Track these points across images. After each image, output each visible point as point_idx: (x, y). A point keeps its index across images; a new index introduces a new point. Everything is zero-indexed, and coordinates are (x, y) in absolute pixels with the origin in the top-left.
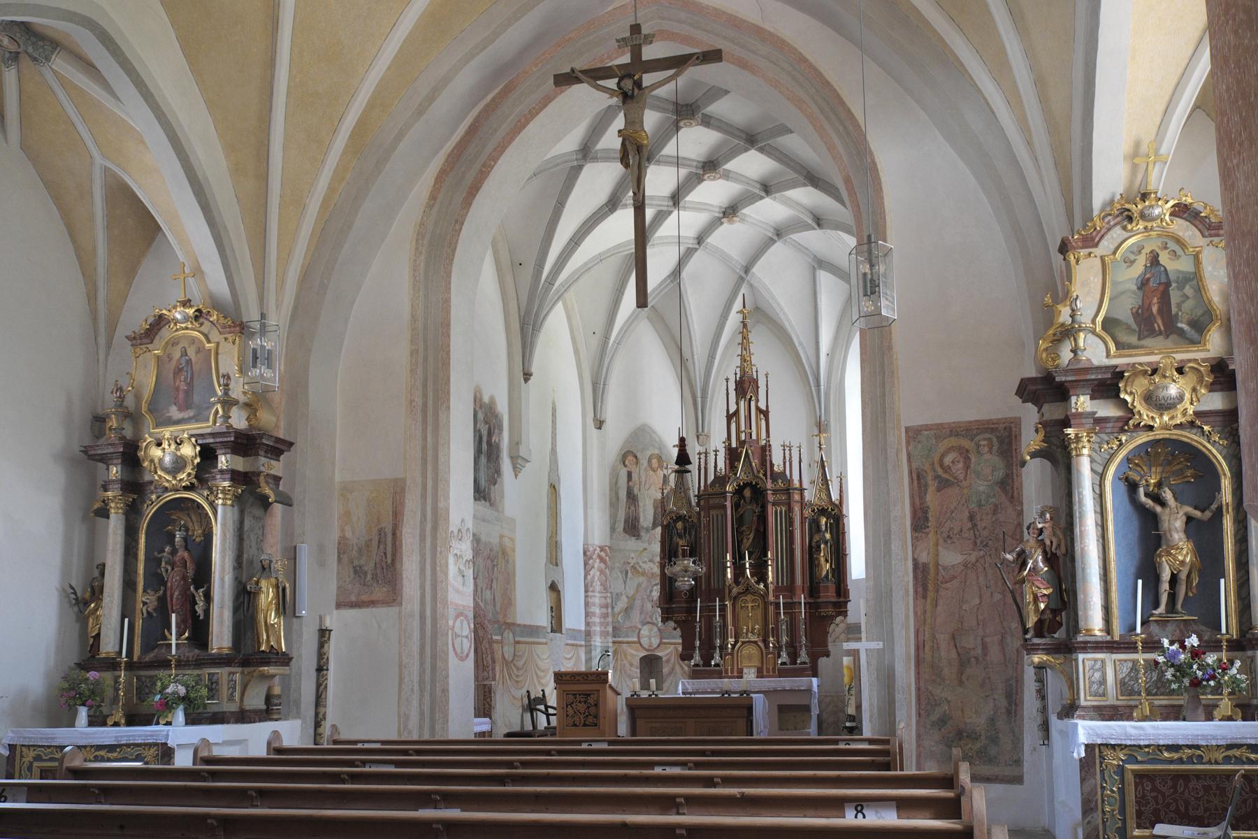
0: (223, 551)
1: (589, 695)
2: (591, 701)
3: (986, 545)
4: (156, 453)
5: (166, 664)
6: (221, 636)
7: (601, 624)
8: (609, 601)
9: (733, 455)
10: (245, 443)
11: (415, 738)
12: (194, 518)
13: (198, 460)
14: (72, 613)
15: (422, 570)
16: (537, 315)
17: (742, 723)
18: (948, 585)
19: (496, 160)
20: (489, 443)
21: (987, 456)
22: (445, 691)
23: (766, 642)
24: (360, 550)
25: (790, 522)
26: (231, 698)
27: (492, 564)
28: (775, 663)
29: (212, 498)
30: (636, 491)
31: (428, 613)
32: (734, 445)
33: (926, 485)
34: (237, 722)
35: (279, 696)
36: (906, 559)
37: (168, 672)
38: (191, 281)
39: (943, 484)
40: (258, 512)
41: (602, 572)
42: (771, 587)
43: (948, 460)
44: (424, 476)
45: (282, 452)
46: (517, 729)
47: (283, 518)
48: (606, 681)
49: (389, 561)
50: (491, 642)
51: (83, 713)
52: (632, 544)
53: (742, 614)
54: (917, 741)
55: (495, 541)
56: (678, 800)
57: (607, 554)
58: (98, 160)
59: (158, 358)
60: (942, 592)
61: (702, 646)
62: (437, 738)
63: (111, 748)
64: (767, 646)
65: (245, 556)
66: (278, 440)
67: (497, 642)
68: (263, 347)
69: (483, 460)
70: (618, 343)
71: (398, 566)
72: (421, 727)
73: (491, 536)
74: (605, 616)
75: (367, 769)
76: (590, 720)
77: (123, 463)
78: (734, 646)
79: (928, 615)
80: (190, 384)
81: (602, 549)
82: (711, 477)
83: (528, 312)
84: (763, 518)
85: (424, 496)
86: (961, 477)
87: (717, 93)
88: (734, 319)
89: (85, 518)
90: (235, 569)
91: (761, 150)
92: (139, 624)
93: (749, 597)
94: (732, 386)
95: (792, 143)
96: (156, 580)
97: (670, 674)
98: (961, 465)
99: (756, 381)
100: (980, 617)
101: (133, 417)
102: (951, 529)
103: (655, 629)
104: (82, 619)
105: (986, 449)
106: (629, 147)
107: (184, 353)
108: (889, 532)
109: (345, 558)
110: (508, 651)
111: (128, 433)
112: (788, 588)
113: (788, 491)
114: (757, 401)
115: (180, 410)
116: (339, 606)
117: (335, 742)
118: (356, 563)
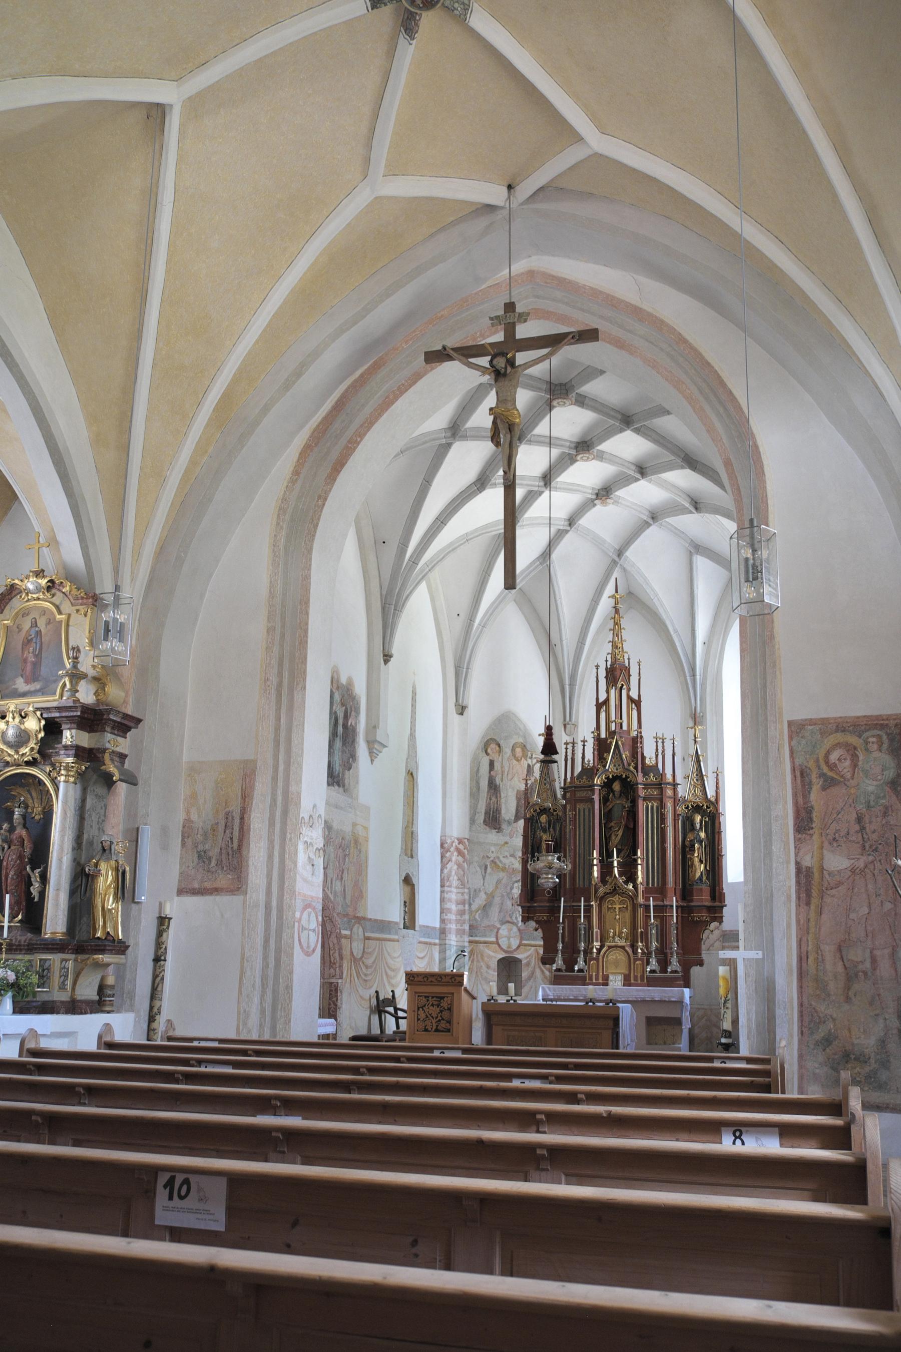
1: (443, 998)
2: (444, 1004)
3: (876, 850)
6: (55, 920)
7: (458, 922)
8: (467, 897)
9: (602, 746)
10: (92, 719)
12: (34, 794)
15: (270, 857)
17: (607, 1035)
18: (833, 892)
19: (362, 436)
20: (345, 726)
21: (877, 754)
22: (289, 988)
23: (634, 947)
24: (205, 835)
25: (662, 819)
26: (62, 987)
27: (344, 853)
28: (644, 971)
29: (54, 774)
30: (498, 781)
31: (274, 903)
32: (603, 735)
33: (810, 783)
35: (112, 987)
36: (788, 862)
38: (45, 550)
39: (829, 783)
40: (100, 790)
41: (459, 866)
42: (641, 888)
43: (834, 757)
44: (276, 758)
46: (363, 1032)
48: (461, 983)
49: (235, 846)
50: (339, 937)
52: (492, 837)
53: (609, 916)
55: (348, 829)
60: (828, 900)
61: (565, 950)
62: (278, 1039)
64: (635, 952)
65: (85, 836)
66: (126, 716)
67: (346, 937)
69: (338, 743)
70: (483, 625)
71: (244, 852)
72: (261, 1026)
73: (344, 824)
74: (462, 913)
75: (202, 1069)
76: (443, 1025)
78: (599, 951)
79: (812, 924)
80: (38, 656)
81: (460, 841)
82: (578, 769)
83: (390, 592)
84: (633, 814)
85: (275, 779)
86: (849, 775)
90: (74, 849)
91: (637, 431)
93: (616, 898)
94: (602, 673)
95: (670, 425)
97: (529, 978)
98: (847, 763)
99: (628, 670)
100: (869, 928)
102: (837, 831)
103: (515, 929)
105: (875, 747)
106: (500, 426)
107: (35, 624)
109: (189, 842)
110: (357, 948)
112: (660, 891)
113: (660, 785)
114: (629, 690)
115: (27, 682)
116: (181, 892)
117: (170, 1039)
118: (200, 847)
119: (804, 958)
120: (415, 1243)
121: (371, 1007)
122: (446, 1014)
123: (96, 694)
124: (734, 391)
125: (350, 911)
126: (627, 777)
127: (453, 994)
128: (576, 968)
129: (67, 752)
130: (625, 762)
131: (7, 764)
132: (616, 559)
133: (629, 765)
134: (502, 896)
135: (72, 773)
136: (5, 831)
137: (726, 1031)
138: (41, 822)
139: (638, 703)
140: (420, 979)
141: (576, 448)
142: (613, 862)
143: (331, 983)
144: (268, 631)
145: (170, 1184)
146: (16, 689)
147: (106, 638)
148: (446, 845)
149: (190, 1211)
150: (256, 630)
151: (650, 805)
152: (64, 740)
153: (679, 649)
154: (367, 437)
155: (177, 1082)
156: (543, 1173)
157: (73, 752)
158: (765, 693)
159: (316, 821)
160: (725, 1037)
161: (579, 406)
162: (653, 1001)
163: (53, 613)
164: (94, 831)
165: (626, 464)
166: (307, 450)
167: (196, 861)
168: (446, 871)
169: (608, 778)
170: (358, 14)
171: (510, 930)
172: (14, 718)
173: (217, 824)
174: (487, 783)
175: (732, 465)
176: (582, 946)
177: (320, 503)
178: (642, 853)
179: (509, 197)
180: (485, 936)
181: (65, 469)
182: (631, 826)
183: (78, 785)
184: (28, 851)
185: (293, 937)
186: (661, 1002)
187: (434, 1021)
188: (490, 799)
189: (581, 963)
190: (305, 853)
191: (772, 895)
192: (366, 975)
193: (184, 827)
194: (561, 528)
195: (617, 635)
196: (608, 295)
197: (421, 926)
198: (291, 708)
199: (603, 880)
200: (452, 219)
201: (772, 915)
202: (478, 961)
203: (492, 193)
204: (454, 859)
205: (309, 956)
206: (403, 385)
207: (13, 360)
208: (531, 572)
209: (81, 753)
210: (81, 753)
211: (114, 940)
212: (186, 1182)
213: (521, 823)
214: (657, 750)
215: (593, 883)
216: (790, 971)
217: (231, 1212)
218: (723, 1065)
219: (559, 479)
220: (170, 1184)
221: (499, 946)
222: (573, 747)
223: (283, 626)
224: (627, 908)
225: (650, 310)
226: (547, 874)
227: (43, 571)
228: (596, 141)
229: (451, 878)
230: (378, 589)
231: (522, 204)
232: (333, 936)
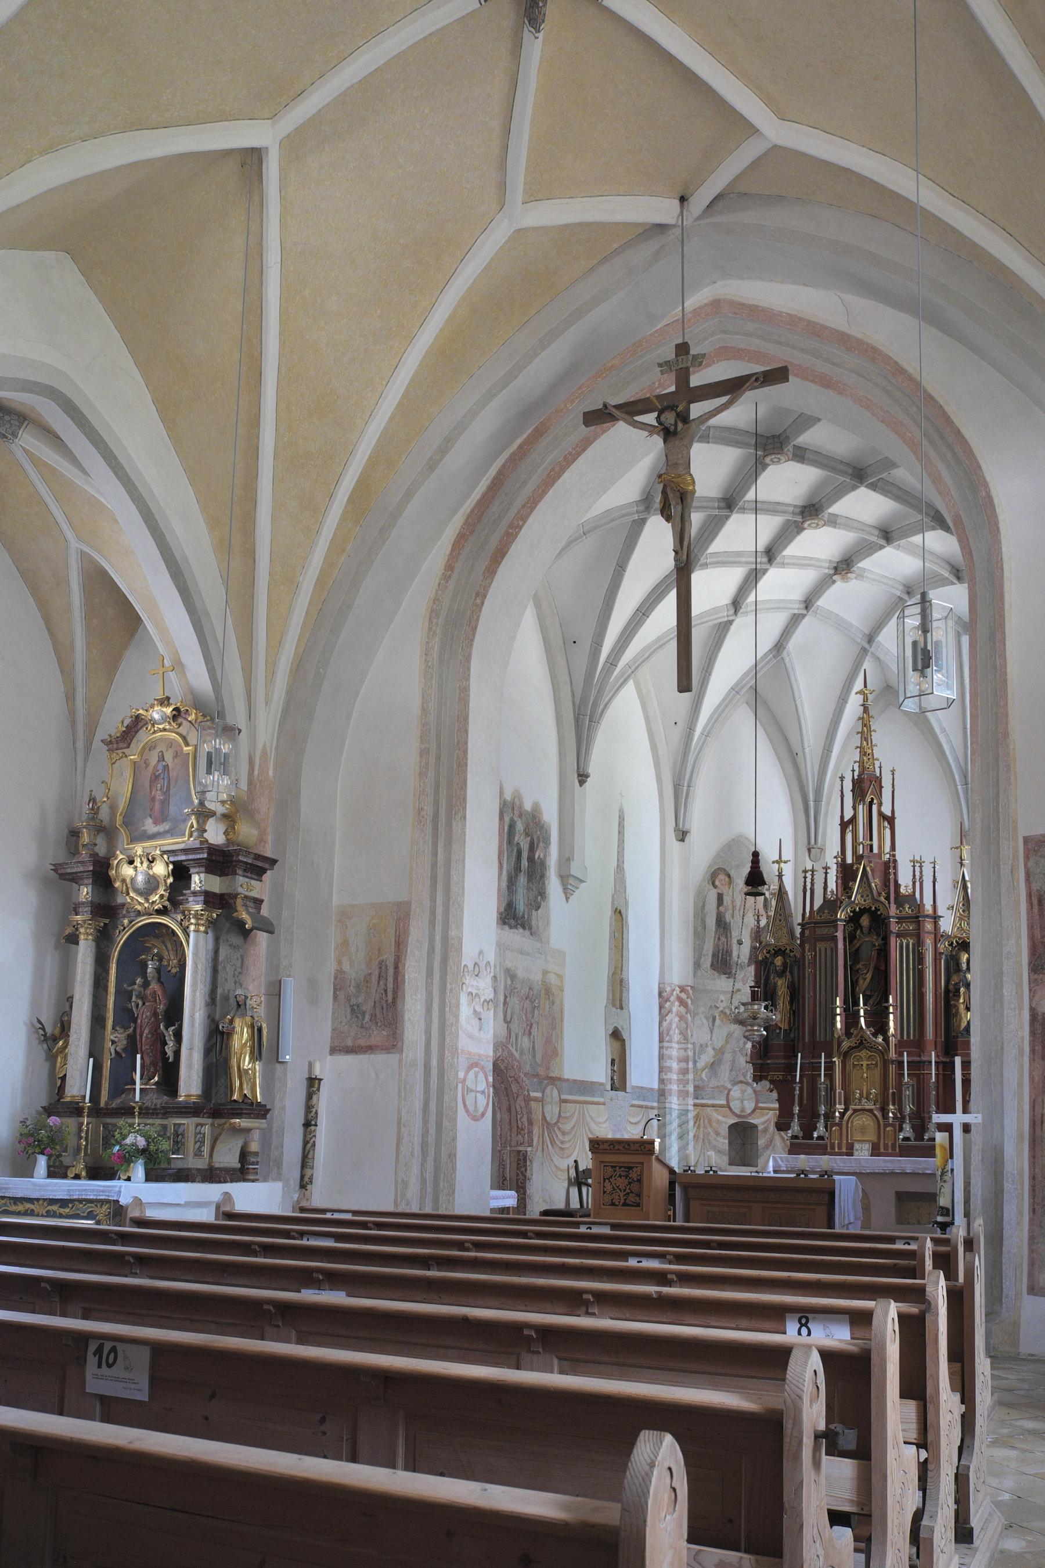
0: (194, 985)
1: (631, 1168)
2: (633, 1175)
4: (127, 871)
5: (129, 1112)
6: (190, 1082)
7: (680, 1081)
8: (690, 1053)
9: (847, 873)
10: (220, 861)
11: (415, 1209)
12: (169, 946)
13: (171, 880)
14: (40, 1051)
15: (429, 1010)
16: (595, 704)
17: (821, 1211)
19: (524, 519)
20: (531, 859)
22: (452, 1156)
23: (884, 1110)
24: (358, 986)
25: (920, 959)
26: (198, 1153)
27: (529, 1006)
28: (896, 1138)
29: (185, 923)
30: (728, 917)
31: (434, 1062)
32: (849, 861)
34: (204, 1180)
35: (256, 1154)
36: (1021, 1008)
37: (130, 1121)
38: (172, 675)
40: (236, 939)
41: (681, 1018)
42: (892, 1041)
44: (433, 899)
45: (264, 871)
46: (561, 1205)
47: (268, 946)
48: (651, 1151)
49: (390, 998)
50: (528, 1100)
51: (42, 1162)
52: (723, 984)
53: (855, 1074)
54: (1030, 1245)
55: (536, 977)
56: (585, 1296)
57: (689, 997)
58: (74, 544)
61: (804, 1115)
62: (440, 1212)
63: (63, 1203)
64: (885, 1117)
65: (219, 991)
66: (258, 857)
67: (536, 1099)
68: (218, 751)
69: (522, 879)
70: (707, 734)
71: (399, 1007)
72: (422, 1198)
73: (530, 970)
74: (684, 1072)
75: (304, 1242)
76: (632, 1198)
77: (94, 883)
78: (842, 1115)
80: (167, 793)
81: (683, 989)
82: (818, 902)
83: (584, 700)
84: (884, 953)
85: (432, 923)
87: (806, 421)
88: (854, 702)
89: (57, 946)
90: (207, 1005)
91: (873, 487)
92: (107, 1064)
93: (864, 1053)
94: (848, 785)
95: (901, 475)
96: (126, 1017)
97: (767, 1146)
99: (879, 780)
101: (108, 832)
103: (749, 1090)
104: (51, 1057)
106: (671, 495)
107: (162, 758)
108: (1001, 974)
109: (341, 995)
110: (551, 1112)
111: (101, 850)
112: (915, 1044)
113: (917, 917)
114: (880, 804)
115: (156, 823)
116: (333, 1051)
117: (302, 1210)
118: (353, 1001)
119: (1038, 1122)
120: (323, 1420)
121: (569, 1179)
122: (635, 1187)
123: (226, 833)
124: (963, 430)
125: (541, 1071)
126: (877, 910)
127: (642, 1163)
128: (815, 1135)
129: (197, 899)
130: (875, 891)
131: (139, 914)
132: (867, 646)
133: (879, 894)
134: (734, 1052)
135: (202, 922)
136: (140, 986)
137: (942, 1208)
139: (891, 820)
140: (606, 1146)
141: (802, 513)
142: (859, 1011)
143: (519, 1152)
144: (421, 756)
145: (99, 1351)
146: (145, 831)
147: (209, 771)
148: (665, 994)
149: (117, 1380)
150: (408, 754)
151: (905, 942)
152: (193, 885)
153: (948, 752)
154: (531, 520)
155: (255, 1254)
156: (535, 1356)
157: (202, 898)
158: (998, 803)
159: (482, 968)
160: (942, 1215)
161: (798, 462)
162: (904, 1174)
163: (180, 745)
164: (230, 985)
165: (867, 529)
166: (461, 539)
167: (349, 1017)
168: (665, 1024)
169: (854, 912)
170: (470, 9)
171: (743, 1092)
172: (142, 863)
173: (370, 974)
174: (714, 920)
175: (962, 523)
176: (822, 1109)
177: (478, 601)
178: (895, 1000)
179: (682, 213)
180: (714, 1098)
181: (185, 582)
182: (883, 968)
183: (211, 935)
184: (161, 1008)
185: (456, 1100)
186: (913, 1174)
187: (622, 1194)
188: (719, 939)
189: (821, 1130)
190: (469, 1005)
191: (1002, 1049)
192: (562, 1142)
193: (335, 978)
194: (796, 612)
195: (866, 739)
196: (809, 322)
197: (633, 1087)
198: (449, 842)
199: (848, 1033)
200: (615, 246)
201: (1002, 1072)
202: (705, 1127)
203: (663, 209)
204: (674, 1009)
205: (477, 1120)
206: (570, 454)
207: (118, 463)
209: (211, 899)
210: (211, 899)
211: (252, 1103)
212: (114, 1350)
213: (753, 967)
214: (914, 875)
215: (836, 1036)
216: (1021, 1137)
217: (153, 1381)
218: (906, 1247)
219: (785, 553)
220: (99, 1351)
221: (730, 1109)
222: (813, 875)
223: (439, 747)
224: (876, 1065)
225: (860, 336)
226: (752, 1025)
227: (168, 698)
228: (774, 130)
229: (671, 1032)
230: (569, 698)
231: (698, 219)
232: (521, 1098)
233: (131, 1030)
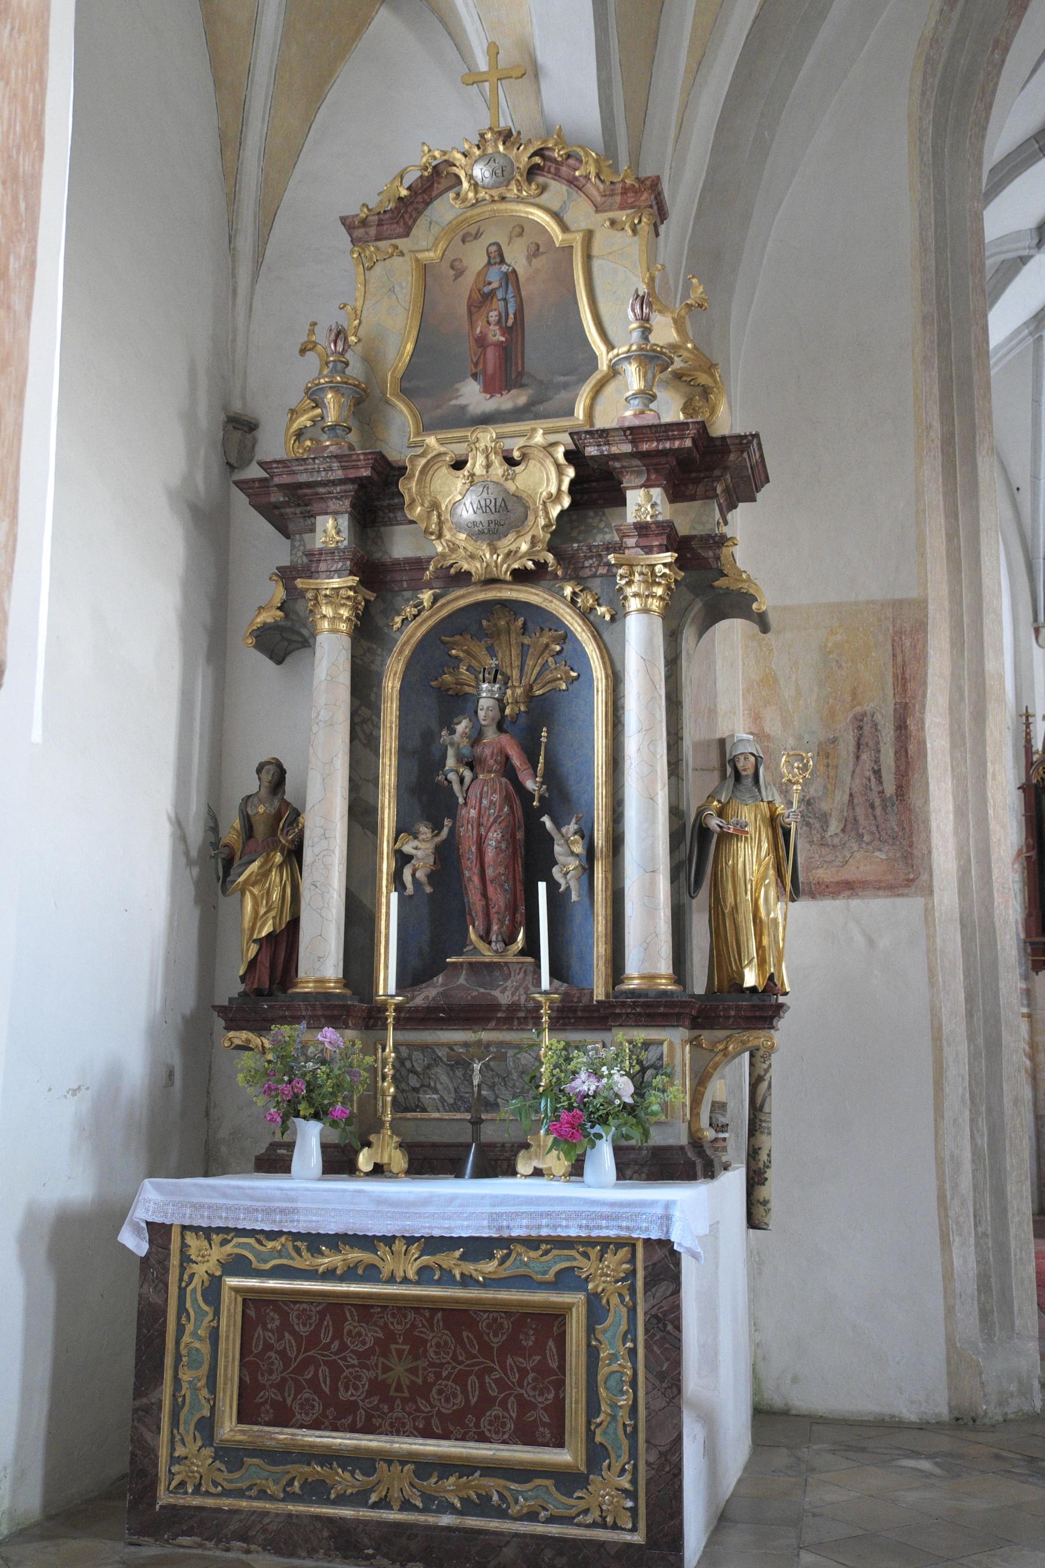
29: (586, 600)
49: (890, 789)
51: (310, 1139)
59: (425, 270)
71: (915, 799)
115: (490, 388)
138: (523, 720)
146: (463, 408)
173: (834, 741)
208: (1012, 349)
233: (445, 831)
